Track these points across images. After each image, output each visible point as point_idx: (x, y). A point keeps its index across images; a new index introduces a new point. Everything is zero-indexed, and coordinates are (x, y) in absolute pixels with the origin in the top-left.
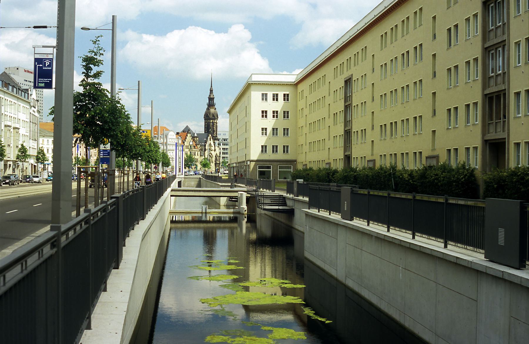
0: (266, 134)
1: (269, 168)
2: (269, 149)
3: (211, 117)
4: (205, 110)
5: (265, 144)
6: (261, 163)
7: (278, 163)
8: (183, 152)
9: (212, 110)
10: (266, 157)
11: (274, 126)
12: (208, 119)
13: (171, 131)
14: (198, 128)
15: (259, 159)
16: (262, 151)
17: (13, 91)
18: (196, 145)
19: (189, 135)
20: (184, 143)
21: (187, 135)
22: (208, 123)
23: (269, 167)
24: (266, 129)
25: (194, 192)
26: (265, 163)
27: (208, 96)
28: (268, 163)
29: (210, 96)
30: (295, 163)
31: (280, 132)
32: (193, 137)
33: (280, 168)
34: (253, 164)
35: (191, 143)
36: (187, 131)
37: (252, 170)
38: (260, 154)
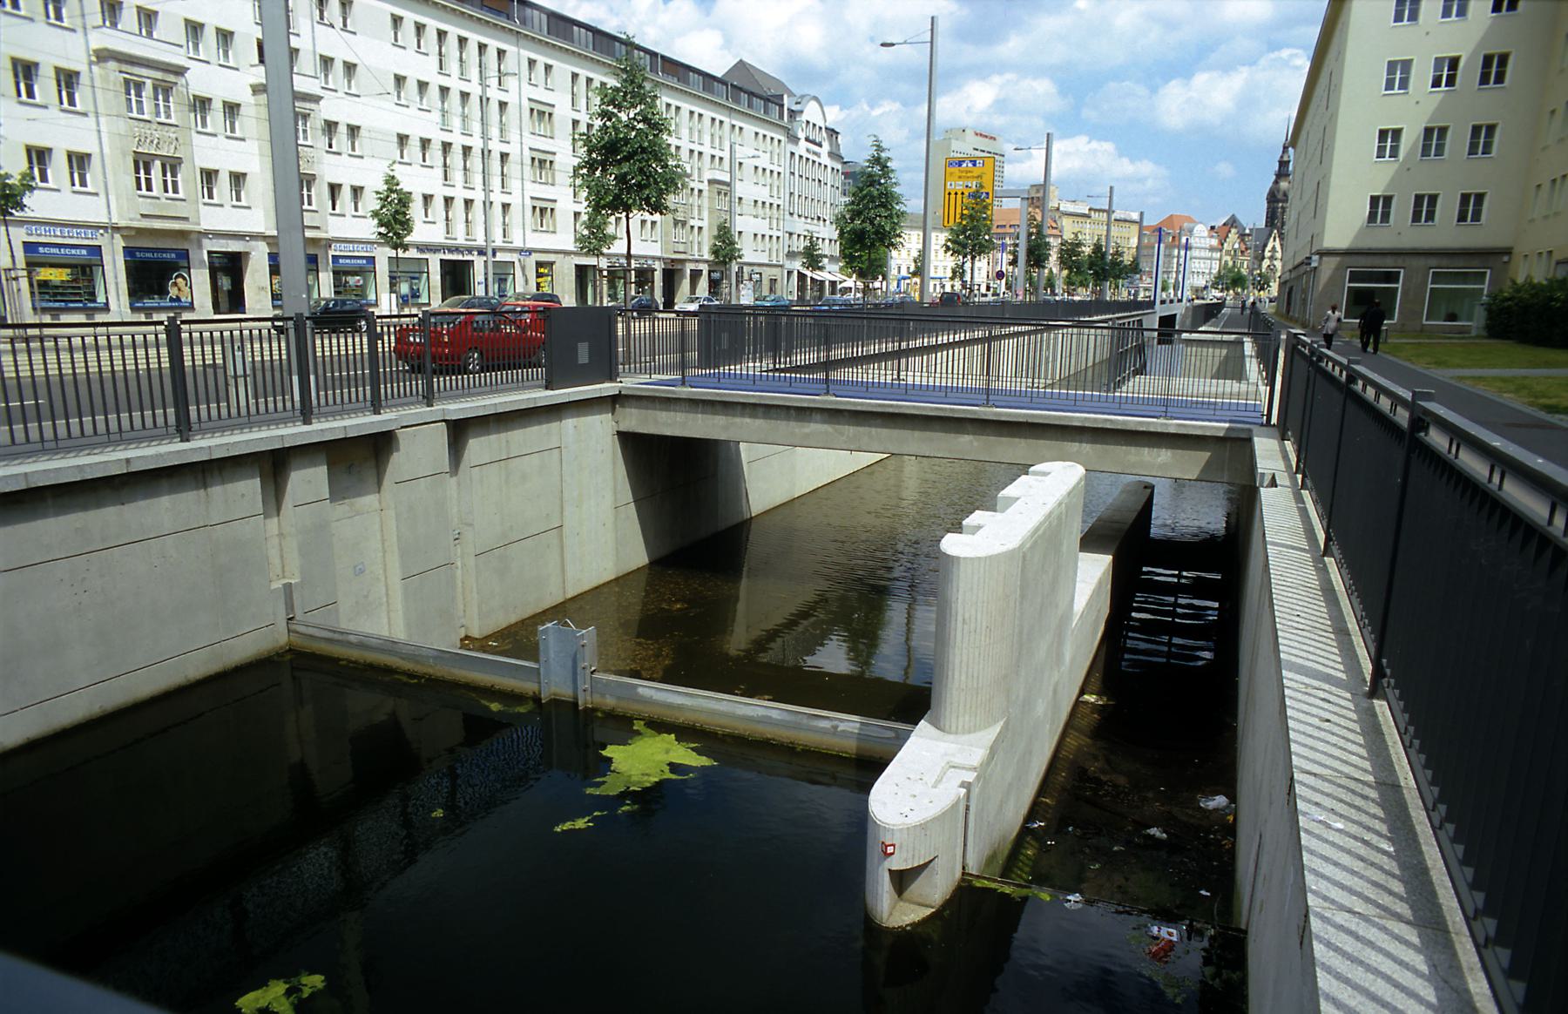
0: (1394, 153)
1: (1392, 277)
2: (1402, 210)
3: (1280, 196)
4: (1270, 184)
5: (1384, 191)
6: (1362, 261)
7: (1433, 261)
8: (1162, 245)
9: (1284, 185)
10: (1384, 238)
11: (1431, 120)
12: (1274, 202)
13: (1201, 223)
14: (1255, 216)
15: (1354, 246)
16: (1372, 217)
17: (750, 105)
18: (1247, 249)
19: (1233, 231)
20: (1222, 245)
21: (1230, 231)
22: (1274, 208)
23: (1391, 277)
24: (1397, 133)
25: (766, 416)
26: (1377, 261)
27: (1278, 158)
28: (1389, 261)
29: (1282, 157)
30: (1506, 258)
31: (1458, 140)
32: (1242, 236)
33: (1437, 278)
34: (1330, 264)
35: (1236, 246)
36: (1233, 222)
37: (1326, 286)
38: (1362, 227)
